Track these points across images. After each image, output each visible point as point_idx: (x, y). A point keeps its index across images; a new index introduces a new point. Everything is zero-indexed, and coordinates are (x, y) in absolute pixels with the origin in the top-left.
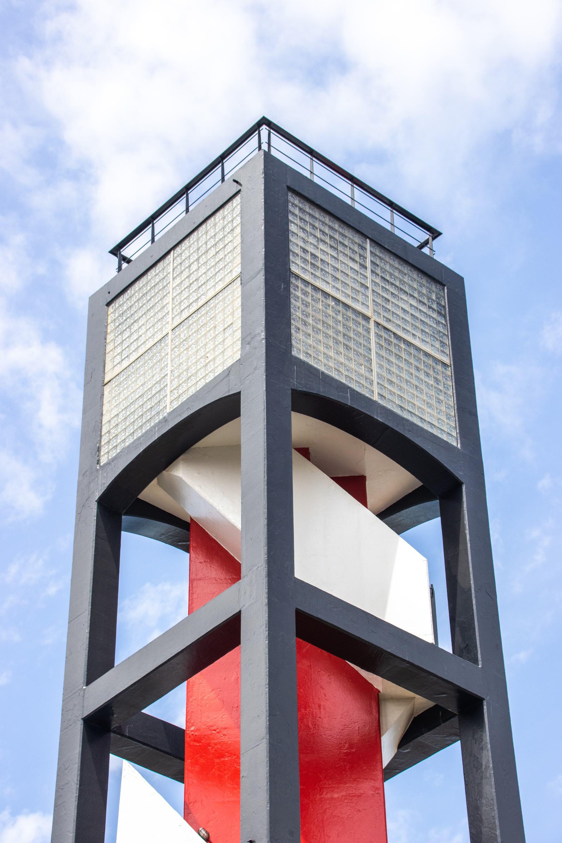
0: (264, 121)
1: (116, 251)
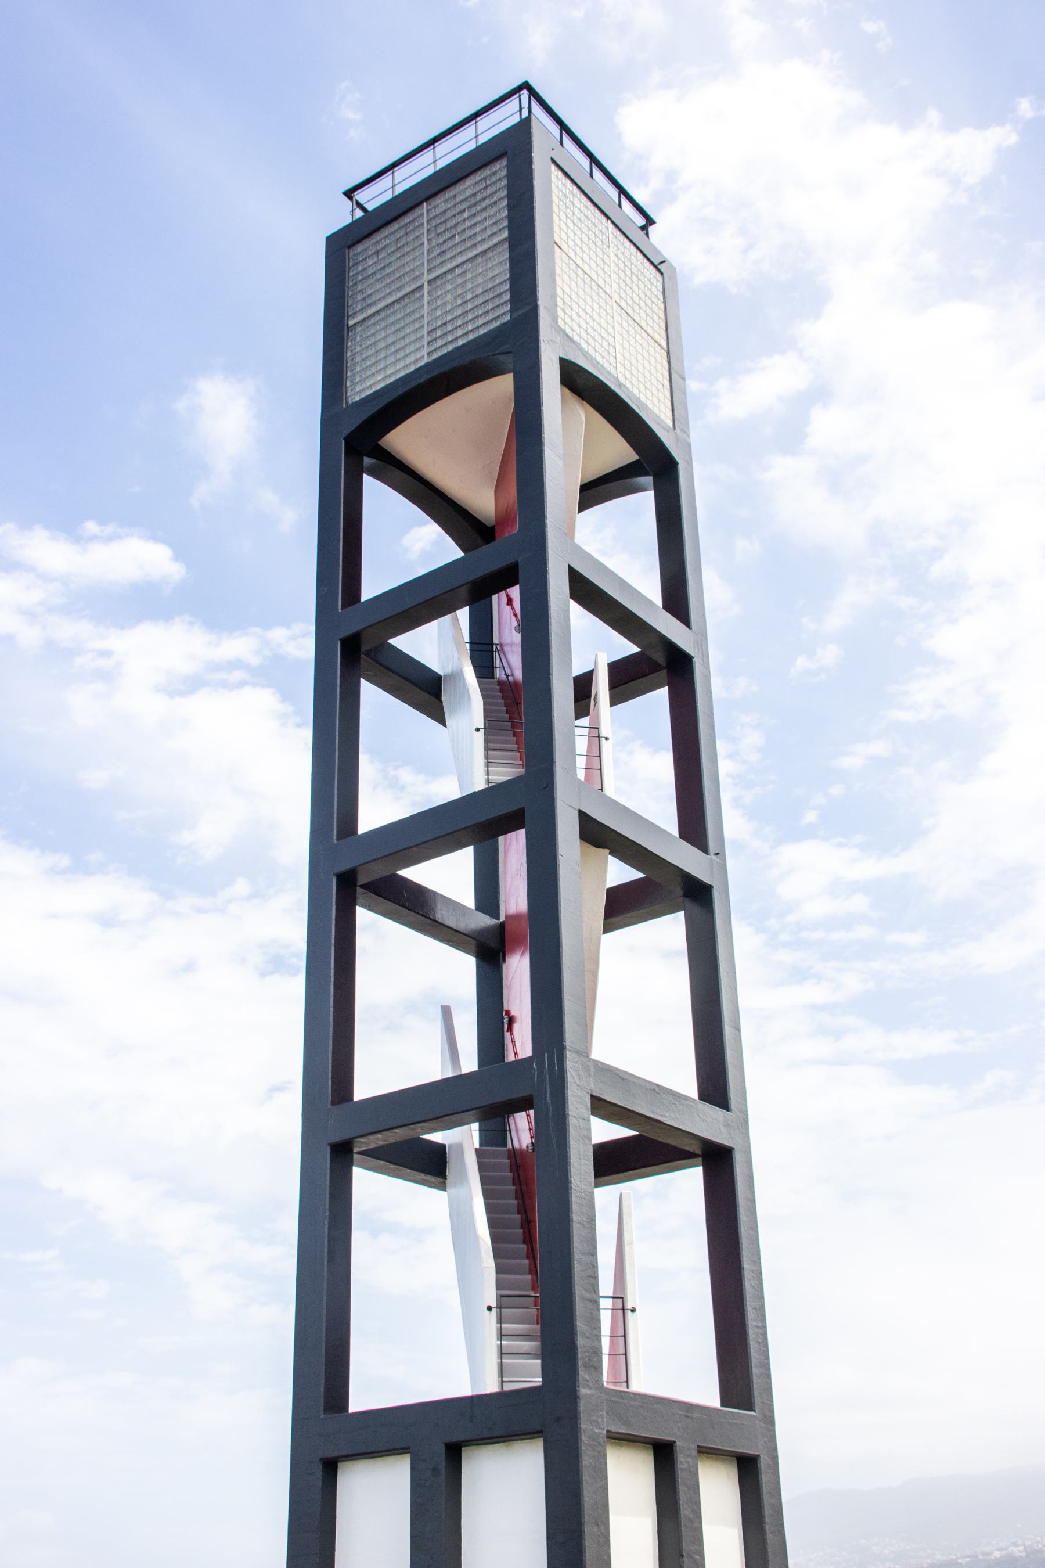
0: (526, 86)
1: (349, 194)
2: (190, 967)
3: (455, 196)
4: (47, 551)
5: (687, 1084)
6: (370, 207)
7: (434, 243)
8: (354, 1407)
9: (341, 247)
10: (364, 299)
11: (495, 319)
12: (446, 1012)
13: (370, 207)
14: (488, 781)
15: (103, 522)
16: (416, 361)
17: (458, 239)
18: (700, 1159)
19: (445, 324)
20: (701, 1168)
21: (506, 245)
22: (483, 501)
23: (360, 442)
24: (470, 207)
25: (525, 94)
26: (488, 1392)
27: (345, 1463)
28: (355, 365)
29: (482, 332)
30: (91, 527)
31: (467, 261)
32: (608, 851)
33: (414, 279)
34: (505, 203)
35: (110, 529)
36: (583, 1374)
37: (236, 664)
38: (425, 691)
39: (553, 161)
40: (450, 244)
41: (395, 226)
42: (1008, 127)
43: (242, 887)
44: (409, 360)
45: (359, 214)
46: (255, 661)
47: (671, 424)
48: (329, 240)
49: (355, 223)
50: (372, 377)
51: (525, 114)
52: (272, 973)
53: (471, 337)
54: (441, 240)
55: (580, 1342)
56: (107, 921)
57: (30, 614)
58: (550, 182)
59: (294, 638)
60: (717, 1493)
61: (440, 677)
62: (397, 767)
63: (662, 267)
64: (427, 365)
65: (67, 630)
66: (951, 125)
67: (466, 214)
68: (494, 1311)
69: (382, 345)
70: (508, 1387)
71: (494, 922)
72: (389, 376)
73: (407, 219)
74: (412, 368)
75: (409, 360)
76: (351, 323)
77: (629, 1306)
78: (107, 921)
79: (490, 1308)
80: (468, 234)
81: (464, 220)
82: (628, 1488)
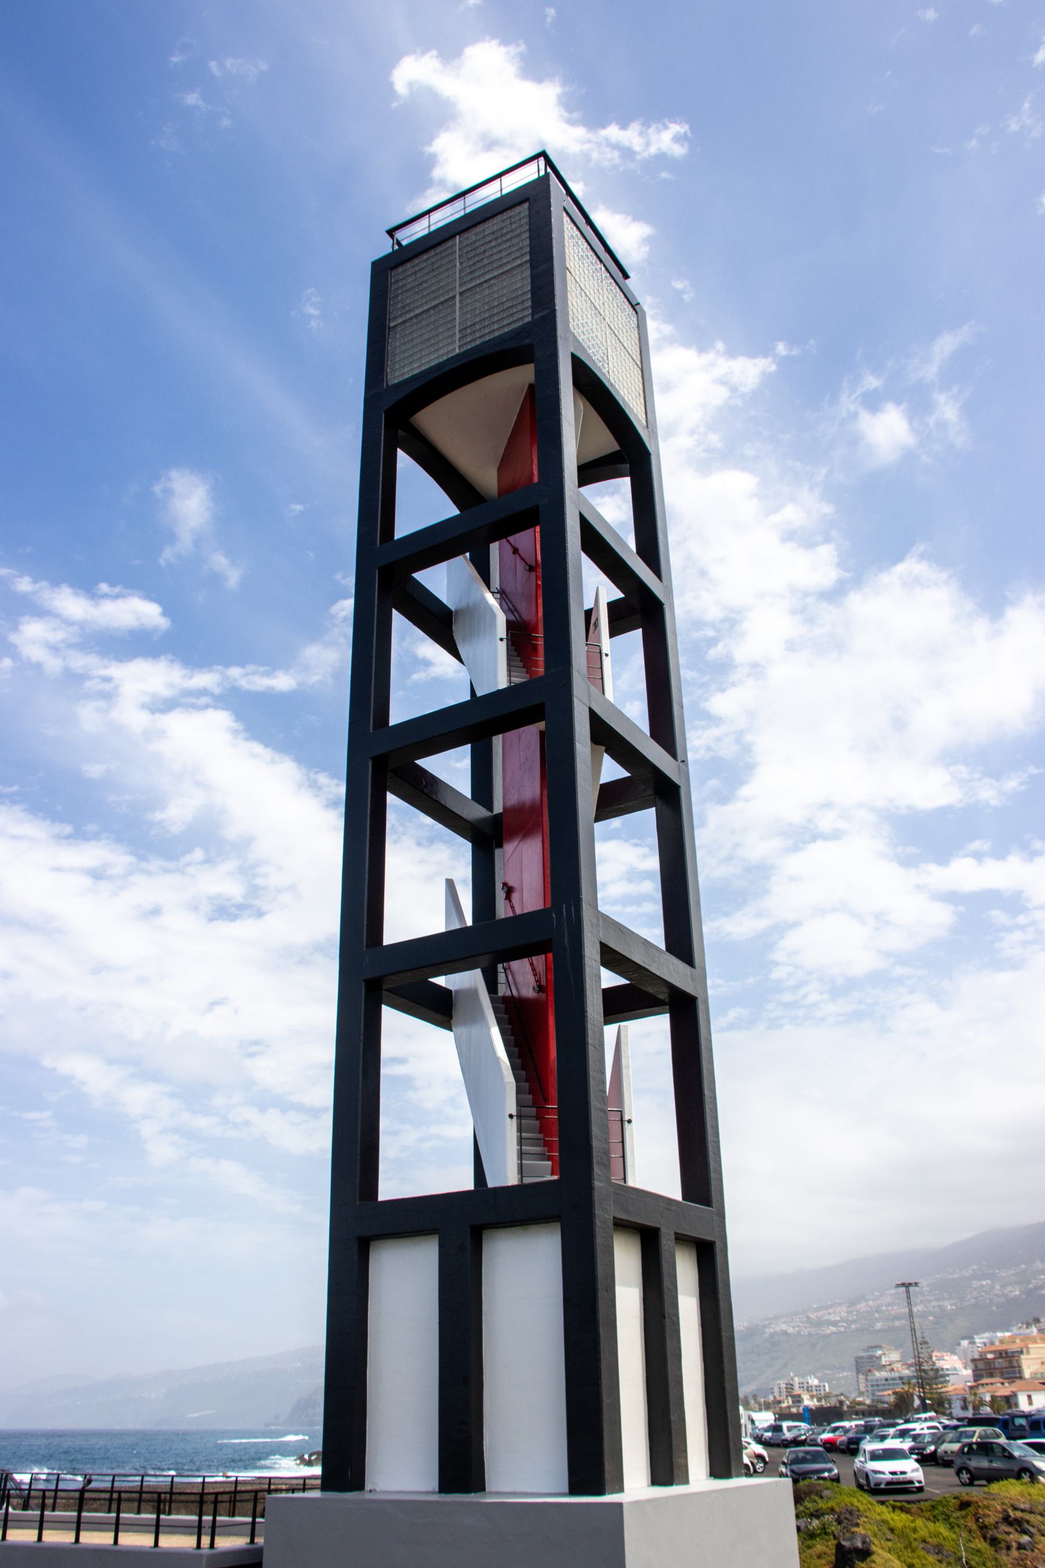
0: (543, 154)
1: (391, 233)
2: (156, 912)
3: (484, 231)
4: (72, 604)
6: (404, 243)
7: (465, 265)
8: (381, 1197)
9: (383, 271)
10: (404, 307)
11: (518, 320)
12: (450, 884)
13: (404, 243)
14: (510, 681)
15: (112, 584)
16: (448, 352)
17: (486, 261)
18: (668, 1007)
19: (474, 324)
20: (668, 1015)
21: (528, 265)
22: (487, 478)
23: (394, 420)
24: (496, 239)
25: (542, 161)
26: (510, 1184)
28: (395, 356)
29: (506, 330)
30: (104, 587)
31: (494, 277)
32: (603, 748)
33: (448, 291)
34: (527, 234)
35: (117, 590)
36: (597, 1170)
37: (203, 692)
38: (440, 624)
39: (565, 209)
40: (478, 265)
41: (432, 253)
42: (770, 359)
43: (198, 854)
44: (441, 352)
46: (217, 691)
48: (375, 264)
49: (394, 253)
50: (408, 364)
51: (542, 173)
52: (217, 919)
53: (497, 334)
54: (471, 263)
55: (595, 1143)
56: (97, 875)
57: (54, 649)
58: (563, 224)
59: (246, 675)
61: (451, 612)
62: (317, 773)
63: (637, 307)
64: (458, 355)
65: (80, 661)
66: (731, 353)
67: (493, 244)
68: (515, 1118)
69: (418, 341)
70: (527, 1181)
71: (489, 814)
72: (424, 364)
73: (441, 248)
74: (445, 358)
75: (441, 352)
76: (392, 324)
77: (626, 1118)
78: (97, 875)
79: (511, 1116)
80: (495, 257)
81: (492, 248)
82: (626, 1265)
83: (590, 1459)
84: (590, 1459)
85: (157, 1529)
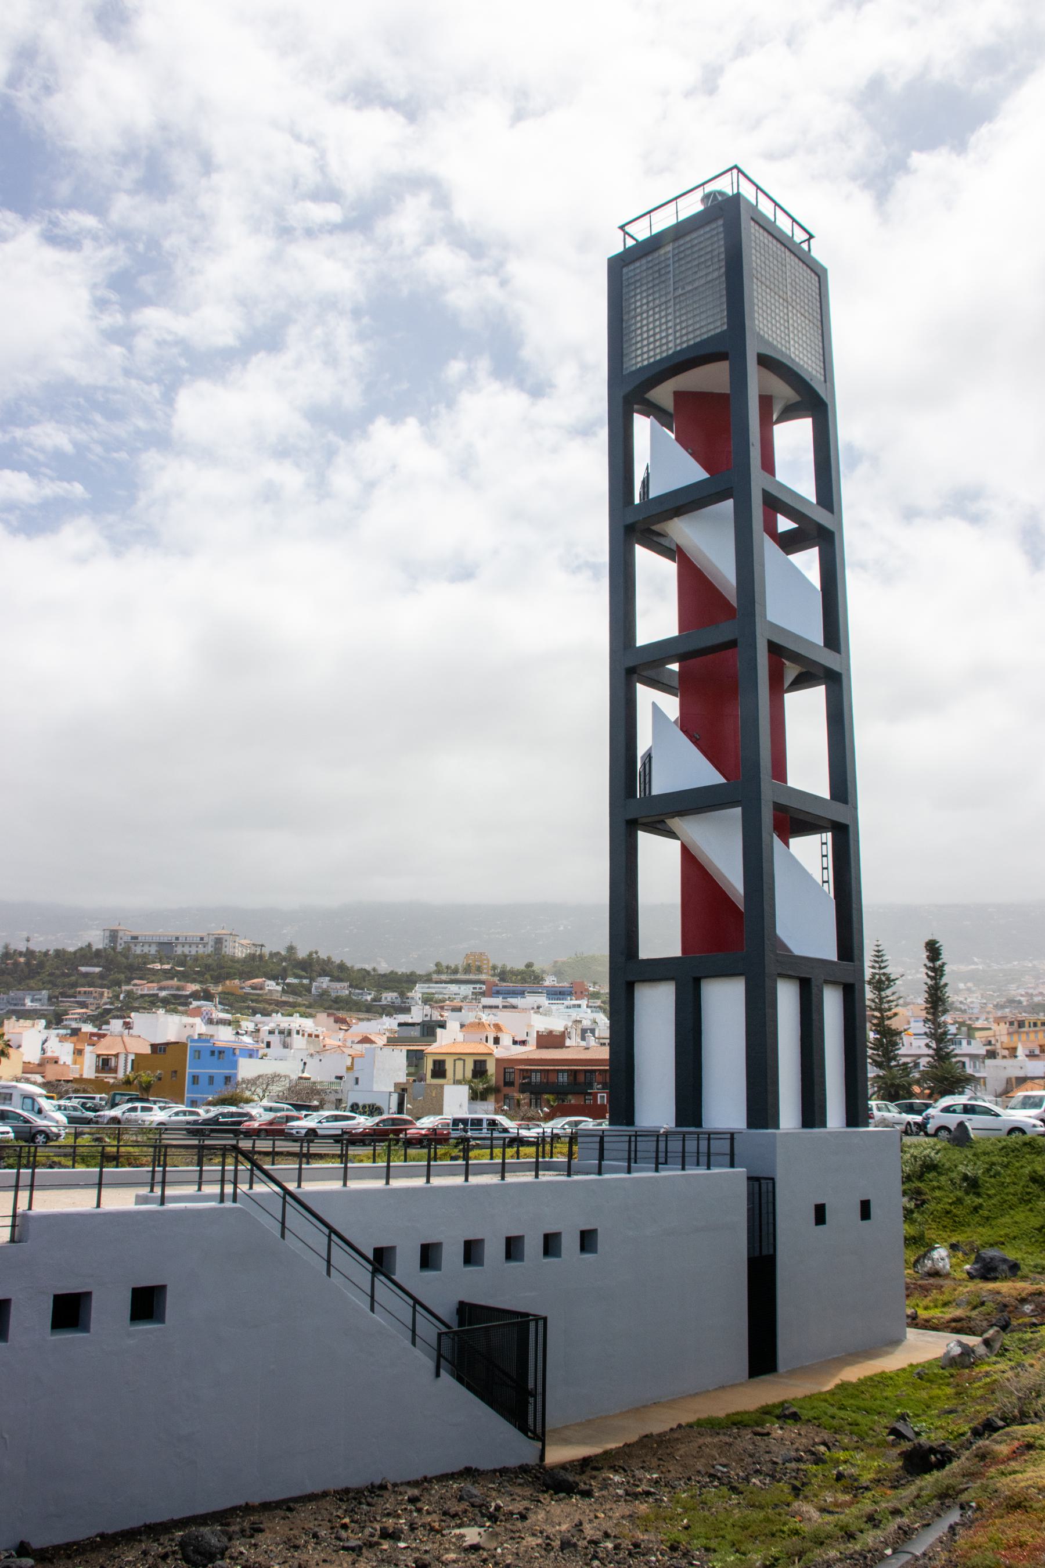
0: (736, 167)
1: (622, 228)
5: (818, 639)
25: (735, 171)
27: (554, 1447)
45: (630, 243)
47: (822, 379)
50: (645, 354)
60: (832, 1003)
82: (787, 999)
83: (761, 1108)
84: (761, 1108)
85: (503, 1170)
